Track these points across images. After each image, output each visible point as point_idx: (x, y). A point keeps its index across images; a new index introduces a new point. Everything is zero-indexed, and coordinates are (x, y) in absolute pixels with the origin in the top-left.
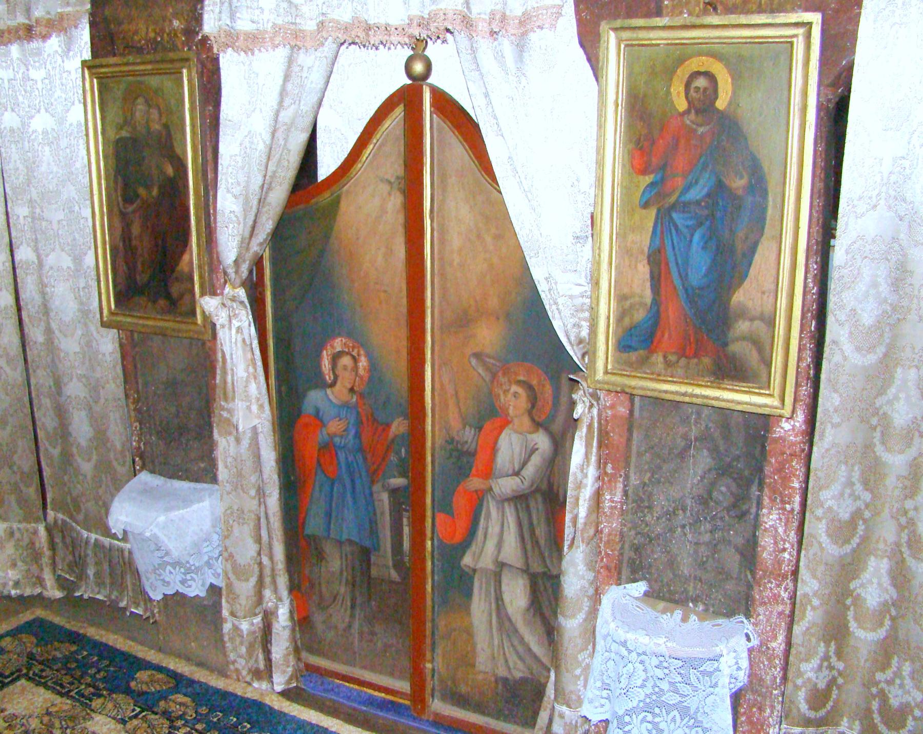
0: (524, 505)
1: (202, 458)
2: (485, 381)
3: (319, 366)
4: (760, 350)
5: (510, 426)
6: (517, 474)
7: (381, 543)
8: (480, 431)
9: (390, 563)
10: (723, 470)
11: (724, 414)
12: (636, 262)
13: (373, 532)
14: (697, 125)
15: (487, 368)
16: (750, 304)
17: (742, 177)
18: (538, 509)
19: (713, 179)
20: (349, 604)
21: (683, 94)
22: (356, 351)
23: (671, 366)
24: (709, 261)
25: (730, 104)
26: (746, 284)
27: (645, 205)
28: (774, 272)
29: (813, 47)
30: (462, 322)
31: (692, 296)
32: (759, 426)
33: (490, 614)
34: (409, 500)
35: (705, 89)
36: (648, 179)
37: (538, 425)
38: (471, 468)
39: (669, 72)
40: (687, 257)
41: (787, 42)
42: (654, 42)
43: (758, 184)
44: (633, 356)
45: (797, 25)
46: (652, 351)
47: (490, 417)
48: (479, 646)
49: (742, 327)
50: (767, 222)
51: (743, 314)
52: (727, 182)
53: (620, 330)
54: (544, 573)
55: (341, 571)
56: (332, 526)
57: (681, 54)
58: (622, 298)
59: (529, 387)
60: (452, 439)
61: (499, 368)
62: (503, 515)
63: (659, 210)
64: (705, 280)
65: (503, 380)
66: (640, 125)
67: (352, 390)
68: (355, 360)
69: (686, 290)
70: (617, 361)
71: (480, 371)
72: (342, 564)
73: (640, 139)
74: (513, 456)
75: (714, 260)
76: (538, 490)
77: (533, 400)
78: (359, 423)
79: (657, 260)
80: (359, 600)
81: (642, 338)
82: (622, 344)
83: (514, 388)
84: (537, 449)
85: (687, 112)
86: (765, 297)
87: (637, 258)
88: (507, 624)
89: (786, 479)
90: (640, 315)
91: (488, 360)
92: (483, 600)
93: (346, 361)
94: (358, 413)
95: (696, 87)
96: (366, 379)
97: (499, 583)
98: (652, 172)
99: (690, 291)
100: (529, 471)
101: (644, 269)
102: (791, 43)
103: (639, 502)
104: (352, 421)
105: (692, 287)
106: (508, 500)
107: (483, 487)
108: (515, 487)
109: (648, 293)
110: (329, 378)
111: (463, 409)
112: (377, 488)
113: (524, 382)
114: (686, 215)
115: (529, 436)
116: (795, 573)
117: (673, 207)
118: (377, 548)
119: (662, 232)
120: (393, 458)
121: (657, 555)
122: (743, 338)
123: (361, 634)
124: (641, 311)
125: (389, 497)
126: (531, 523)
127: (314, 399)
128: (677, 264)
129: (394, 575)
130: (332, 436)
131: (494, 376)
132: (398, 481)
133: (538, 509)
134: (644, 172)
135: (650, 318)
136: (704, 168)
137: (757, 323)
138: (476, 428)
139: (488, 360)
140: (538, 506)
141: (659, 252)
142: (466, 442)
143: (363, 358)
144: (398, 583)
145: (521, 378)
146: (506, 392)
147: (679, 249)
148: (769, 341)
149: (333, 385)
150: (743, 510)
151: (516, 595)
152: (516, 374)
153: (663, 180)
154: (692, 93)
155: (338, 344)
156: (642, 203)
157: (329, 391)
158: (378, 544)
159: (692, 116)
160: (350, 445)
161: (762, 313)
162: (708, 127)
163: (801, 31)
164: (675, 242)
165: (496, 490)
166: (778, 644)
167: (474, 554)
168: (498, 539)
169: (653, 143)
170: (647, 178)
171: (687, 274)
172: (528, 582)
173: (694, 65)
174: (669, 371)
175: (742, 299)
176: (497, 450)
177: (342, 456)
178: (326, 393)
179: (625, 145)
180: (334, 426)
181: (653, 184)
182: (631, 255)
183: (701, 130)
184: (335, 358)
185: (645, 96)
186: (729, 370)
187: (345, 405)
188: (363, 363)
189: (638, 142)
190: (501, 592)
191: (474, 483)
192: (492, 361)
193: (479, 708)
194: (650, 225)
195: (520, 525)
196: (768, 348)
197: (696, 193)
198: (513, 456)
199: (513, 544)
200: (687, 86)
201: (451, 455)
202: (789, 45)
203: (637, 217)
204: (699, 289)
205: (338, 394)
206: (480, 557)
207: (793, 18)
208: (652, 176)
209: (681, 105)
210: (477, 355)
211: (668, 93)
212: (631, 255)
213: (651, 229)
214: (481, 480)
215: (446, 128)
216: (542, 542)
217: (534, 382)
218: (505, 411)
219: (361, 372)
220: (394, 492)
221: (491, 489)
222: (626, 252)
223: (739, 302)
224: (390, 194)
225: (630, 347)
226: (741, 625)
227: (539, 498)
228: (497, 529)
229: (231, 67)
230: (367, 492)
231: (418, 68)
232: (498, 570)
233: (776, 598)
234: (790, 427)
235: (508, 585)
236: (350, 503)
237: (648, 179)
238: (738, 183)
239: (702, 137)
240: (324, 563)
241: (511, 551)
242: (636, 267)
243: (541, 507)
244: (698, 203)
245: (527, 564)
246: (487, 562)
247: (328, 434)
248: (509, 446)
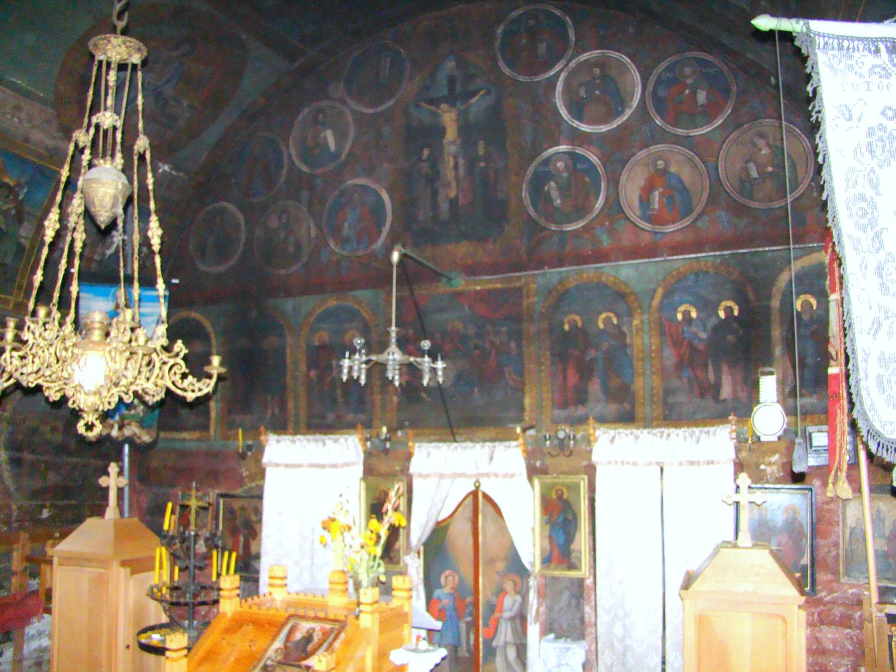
6: (510, 610)
10: (573, 596)
11: (571, 579)
13: (459, 640)
30: (491, 562)
32: (581, 582)
34: (474, 625)
37: (517, 593)
39: (551, 489)
47: (501, 592)
51: (573, 551)
57: (554, 485)
59: (514, 581)
61: (503, 575)
68: (454, 577)
77: (515, 585)
78: (455, 599)
79: (551, 538)
89: (590, 597)
93: (450, 578)
97: (505, 651)
103: (550, 609)
116: (596, 624)
118: (460, 645)
121: (556, 626)
127: (437, 593)
129: (467, 655)
132: (469, 619)
140: (518, 622)
150: (579, 607)
151: (512, 653)
155: (447, 572)
166: (593, 648)
168: (505, 633)
173: (559, 487)
174: (556, 568)
184: (446, 577)
186: (572, 567)
187: (450, 594)
188: (457, 578)
191: (496, 615)
205: (447, 590)
206: (498, 642)
215: (487, 503)
222: (542, 536)
226: (584, 643)
229: (417, 483)
231: (477, 484)
233: (591, 633)
234: (589, 582)
238: (570, 517)
241: (510, 637)
246: (501, 643)
248: (508, 601)
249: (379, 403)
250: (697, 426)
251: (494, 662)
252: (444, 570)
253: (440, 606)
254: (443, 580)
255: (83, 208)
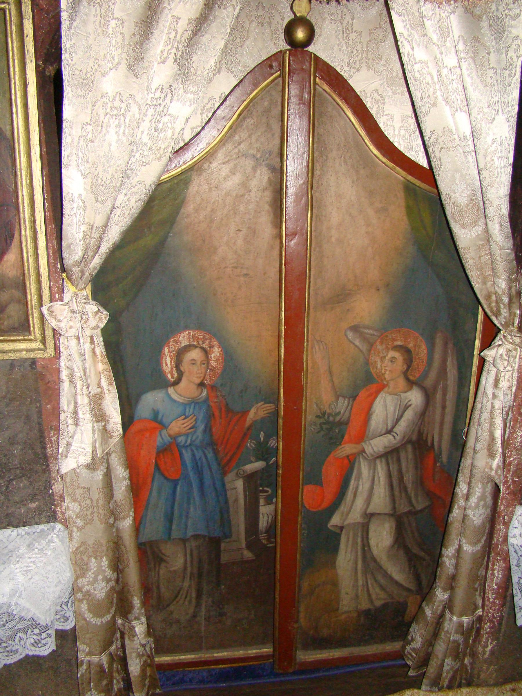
0: (395, 458)
1: (33, 498)
2: (361, 351)
3: (158, 362)
5: (386, 389)
6: (389, 432)
7: (233, 530)
8: (354, 400)
9: (244, 545)
15: (364, 338)
18: (407, 458)
20: (194, 595)
22: (207, 342)
30: (341, 296)
33: (356, 563)
37: (411, 383)
38: (343, 436)
48: (343, 592)
54: (409, 512)
55: (185, 568)
56: (174, 527)
59: (406, 351)
60: (324, 414)
62: (374, 472)
65: (379, 347)
67: (201, 384)
68: (206, 352)
71: (357, 343)
72: (186, 561)
74: (387, 417)
76: (409, 441)
77: (409, 361)
78: (210, 417)
80: (206, 587)
83: (392, 354)
84: (410, 405)
88: (372, 565)
91: (366, 331)
92: (349, 549)
93: (195, 354)
94: (209, 406)
96: (218, 371)
100: (402, 427)
104: (201, 417)
106: (380, 457)
107: (354, 451)
108: (387, 444)
110: (170, 374)
111: (336, 383)
112: (230, 477)
113: (401, 346)
115: (403, 395)
118: (227, 535)
120: (250, 444)
123: (208, 619)
125: (244, 484)
126: (400, 471)
129: (248, 555)
130: (174, 438)
131: (371, 345)
133: (407, 458)
138: (349, 398)
139: (366, 331)
142: (340, 412)
143: (216, 349)
144: (253, 561)
145: (399, 343)
146: (383, 359)
149: (177, 383)
152: (394, 340)
155: (184, 338)
157: (171, 390)
158: (230, 531)
160: (198, 442)
165: (368, 450)
167: (343, 513)
172: (393, 524)
176: (372, 414)
177: (187, 455)
178: (167, 392)
180: (177, 426)
187: (194, 402)
188: (216, 353)
190: (367, 538)
191: (347, 449)
192: (371, 332)
193: (341, 643)
195: (389, 476)
198: (387, 417)
199: (382, 495)
201: (321, 428)
205: (186, 390)
210: (355, 329)
214: (353, 445)
216: (409, 486)
217: (411, 346)
218: (381, 376)
219: (213, 363)
220: (250, 478)
221: (363, 451)
224: (255, 171)
227: (409, 447)
228: (367, 486)
230: (218, 483)
232: (366, 521)
235: (375, 531)
236: (197, 499)
240: (163, 565)
243: (410, 456)
245: (394, 508)
246: (355, 516)
247: (170, 435)
249: (448, 618)
250: (511, 225)
251: (332, 564)
252: (173, 330)
253: (162, 438)
254: (167, 361)
255: (388, 435)
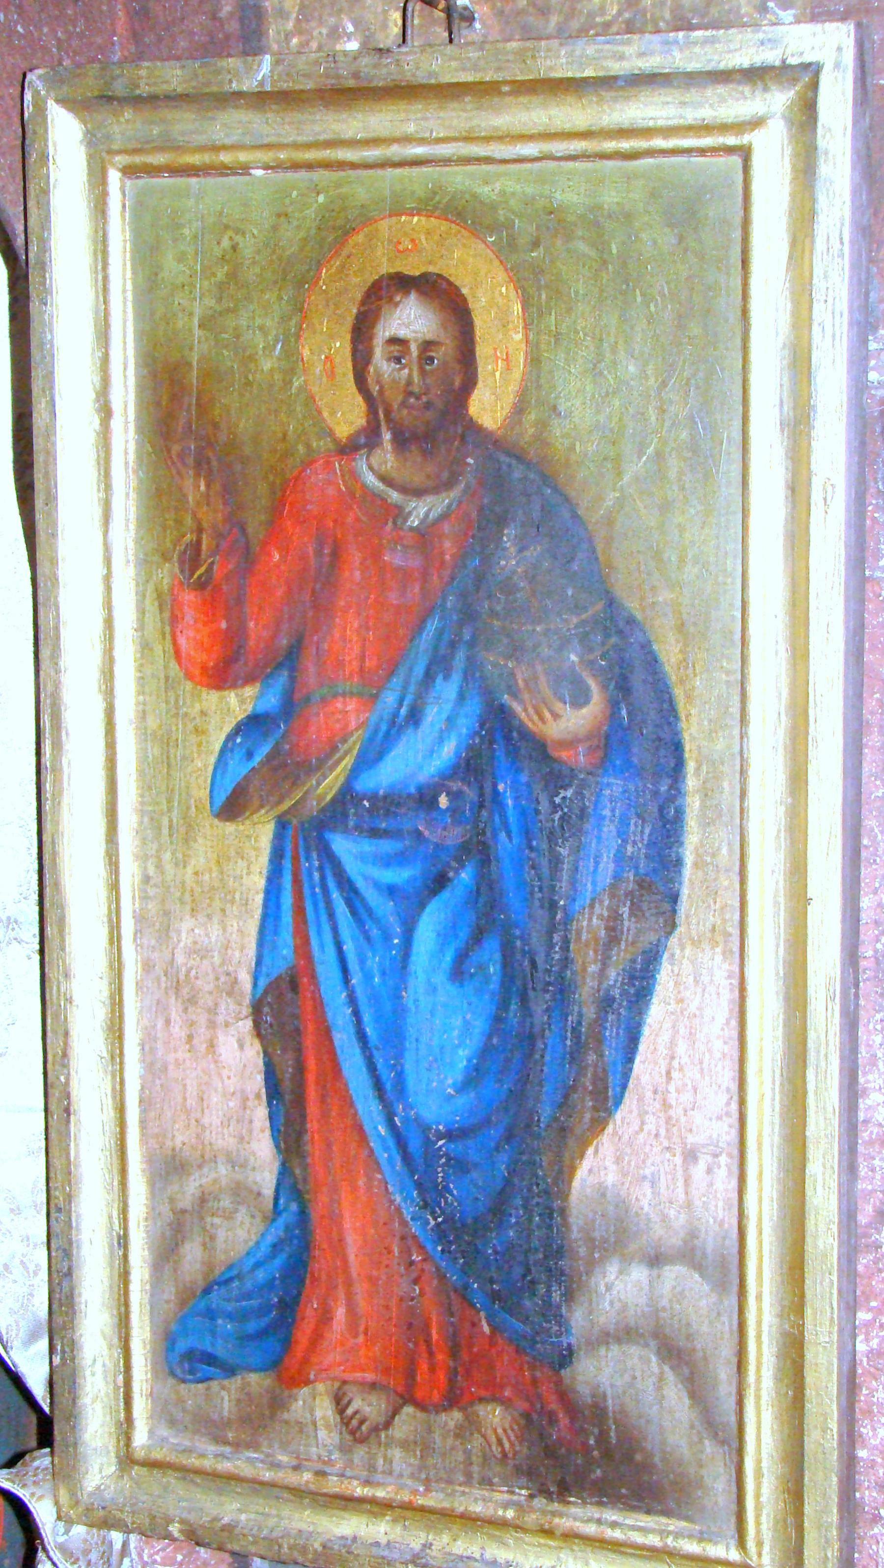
4: (697, 1388)
12: (212, 1025)
14: (404, 490)
16: (643, 1199)
17: (580, 699)
19: (474, 707)
21: (345, 368)
23: (362, 1441)
24: (480, 1026)
25: (519, 409)
26: (625, 1117)
27: (232, 807)
28: (727, 1076)
29: (824, 169)
31: (425, 1159)
35: (427, 345)
36: (238, 703)
40: (400, 1011)
41: (730, 150)
42: (225, 158)
43: (646, 735)
44: (225, 1396)
45: (756, 76)
46: (290, 1374)
49: (619, 1288)
50: (687, 871)
51: (620, 1236)
52: (522, 712)
53: (170, 1292)
58: (169, 1167)
63: (282, 824)
64: (463, 1101)
66: (194, 488)
69: (401, 1142)
70: (165, 1413)
73: (197, 546)
75: (497, 1020)
81: (252, 1326)
82: (183, 1345)
85: (369, 437)
86: (699, 1171)
87: (213, 1011)
90: (240, 1235)
95: (394, 341)
98: (249, 680)
99: (415, 1145)
101: (240, 1055)
102: (745, 153)
105: (425, 1128)
109: (263, 1150)
114: (387, 846)
117: (343, 808)
119: (299, 910)
122: (625, 1334)
123: (191, 349)
124: (242, 1215)
128: (362, 1036)
134: (220, 676)
135: (276, 1248)
136: (438, 665)
137: (672, 1273)
141: (294, 986)
147: (368, 977)
148: (727, 1351)
153: (291, 705)
154: (381, 364)
156: (221, 798)
159: (386, 456)
161: (693, 1234)
162: (455, 493)
163: (778, 100)
164: (349, 947)
169: (250, 561)
170: (232, 697)
171: (400, 1077)
175: (611, 1178)
179: (144, 566)
181: (254, 724)
182: (192, 1000)
183: (420, 511)
185: (210, 374)
189: (191, 558)
194: (257, 882)
196: (724, 1374)
197: (423, 755)
200: (362, 331)
202: (736, 161)
203: (202, 854)
204: (449, 1135)
207: (742, 50)
208: (250, 691)
209: (347, 415)
211: (292, 363)
212: (192, 1000)
213: (259, 898)
223: (602, 1191)
225: (210, 1359)
237: (238, 703)
239: (425, 536)
242: (212, 1046)
244: (425, 799)
